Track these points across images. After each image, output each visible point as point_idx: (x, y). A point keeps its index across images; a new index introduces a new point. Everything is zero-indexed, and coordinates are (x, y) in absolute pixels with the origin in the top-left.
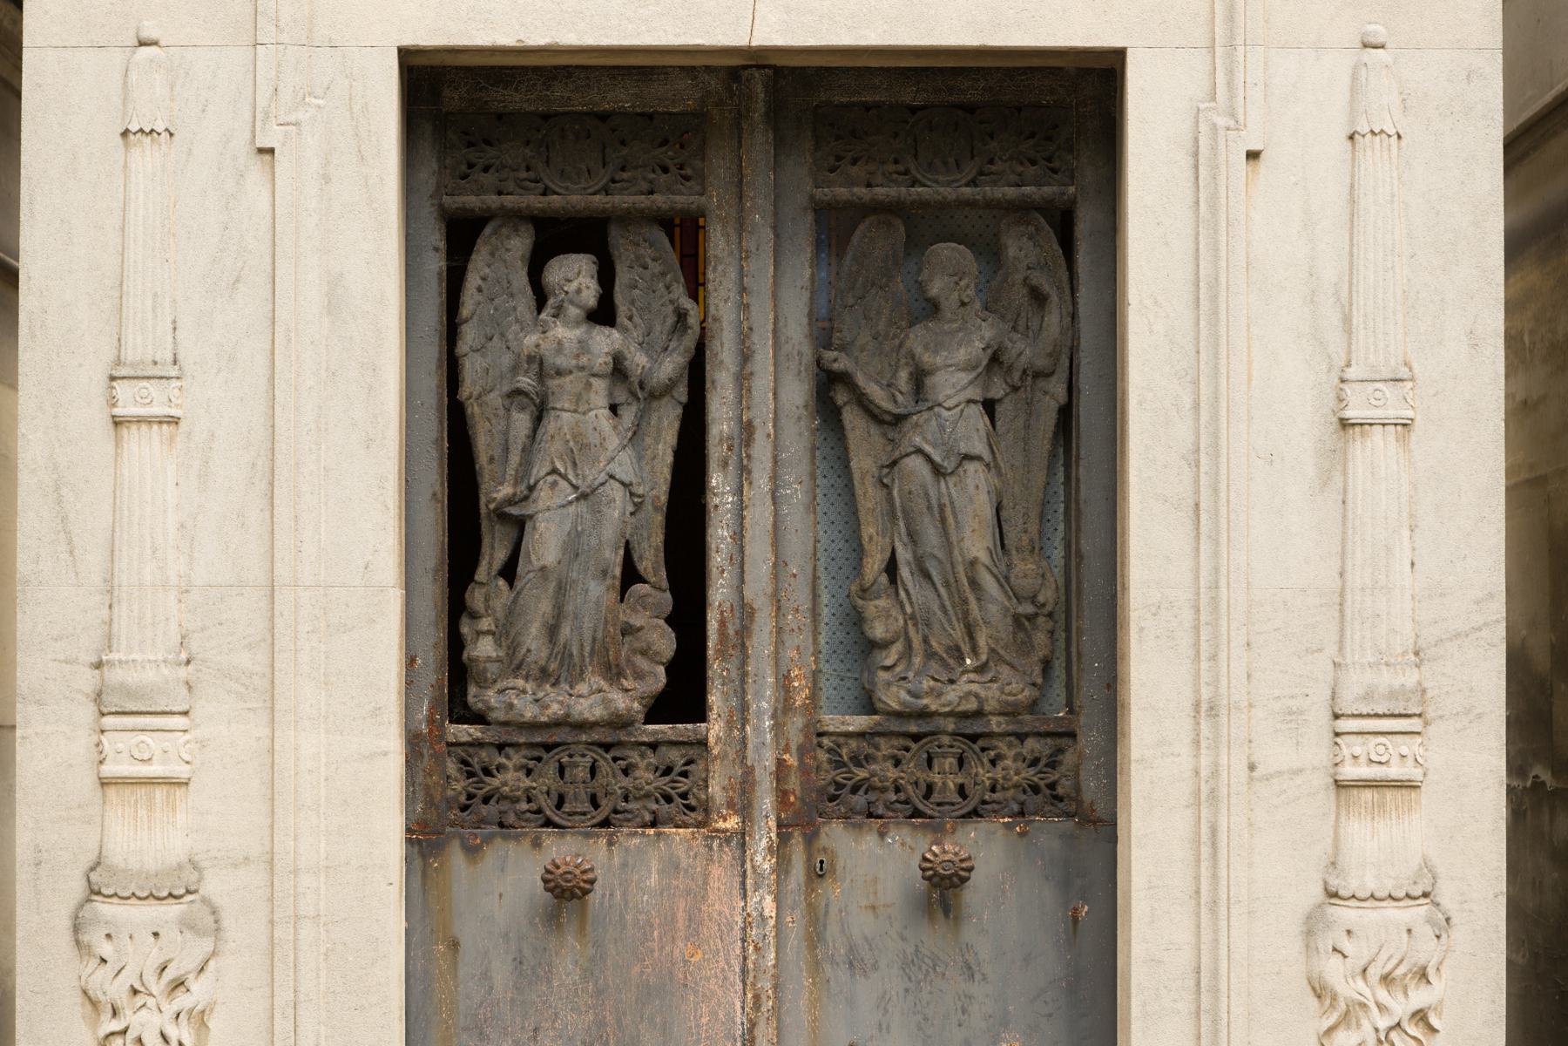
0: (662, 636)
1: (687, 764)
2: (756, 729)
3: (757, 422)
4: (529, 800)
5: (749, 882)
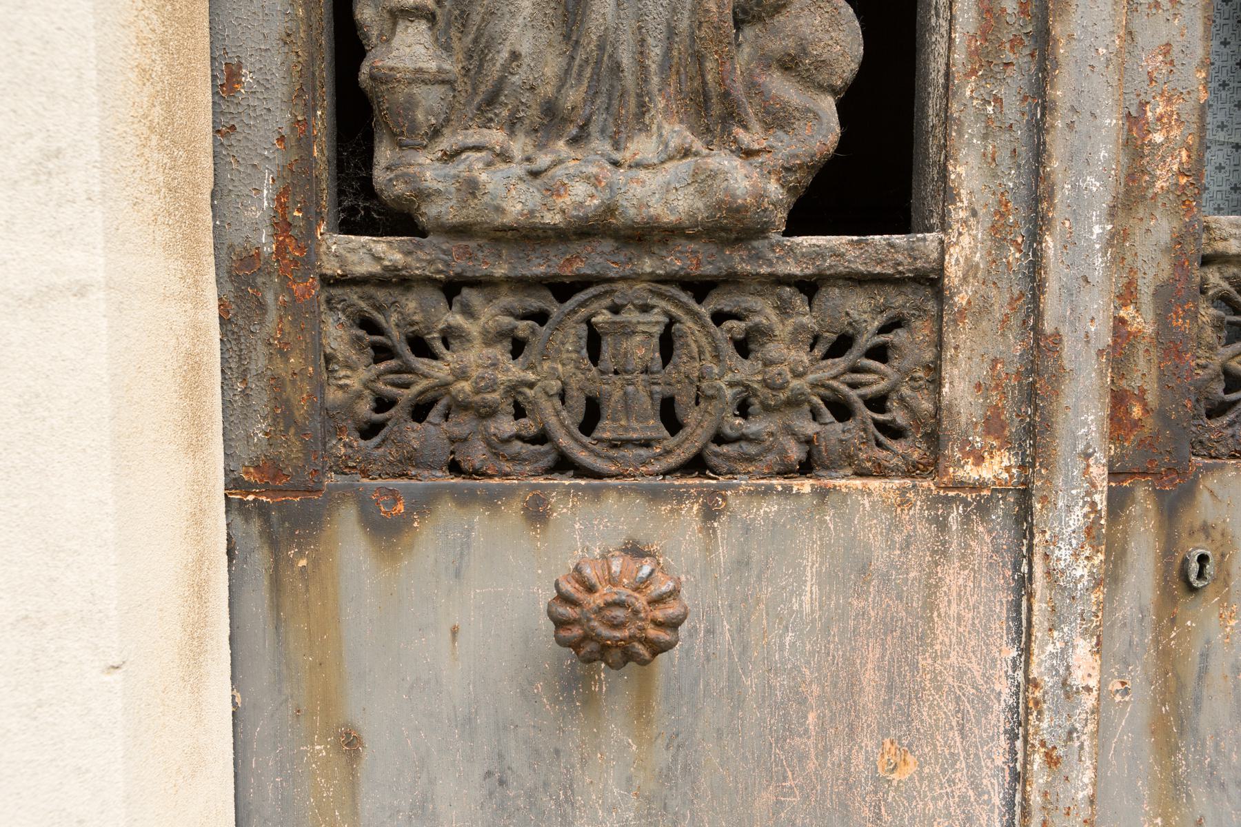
0: (835, 22)
1: (884, 330)
4: (519, 413)
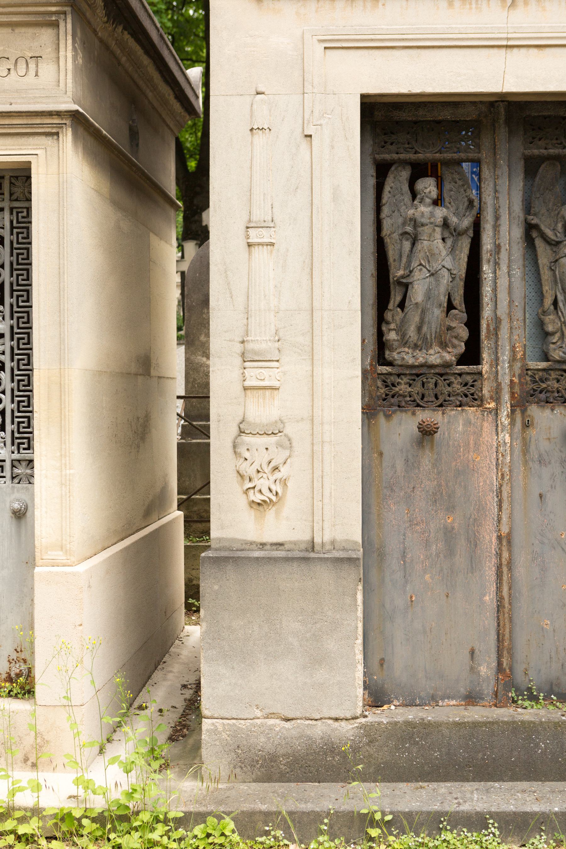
0: (463, 331)
1: (473, 382)
2: (502, 367)
3: (502, 244)
4: (410, 396)
5: (499, 429)
